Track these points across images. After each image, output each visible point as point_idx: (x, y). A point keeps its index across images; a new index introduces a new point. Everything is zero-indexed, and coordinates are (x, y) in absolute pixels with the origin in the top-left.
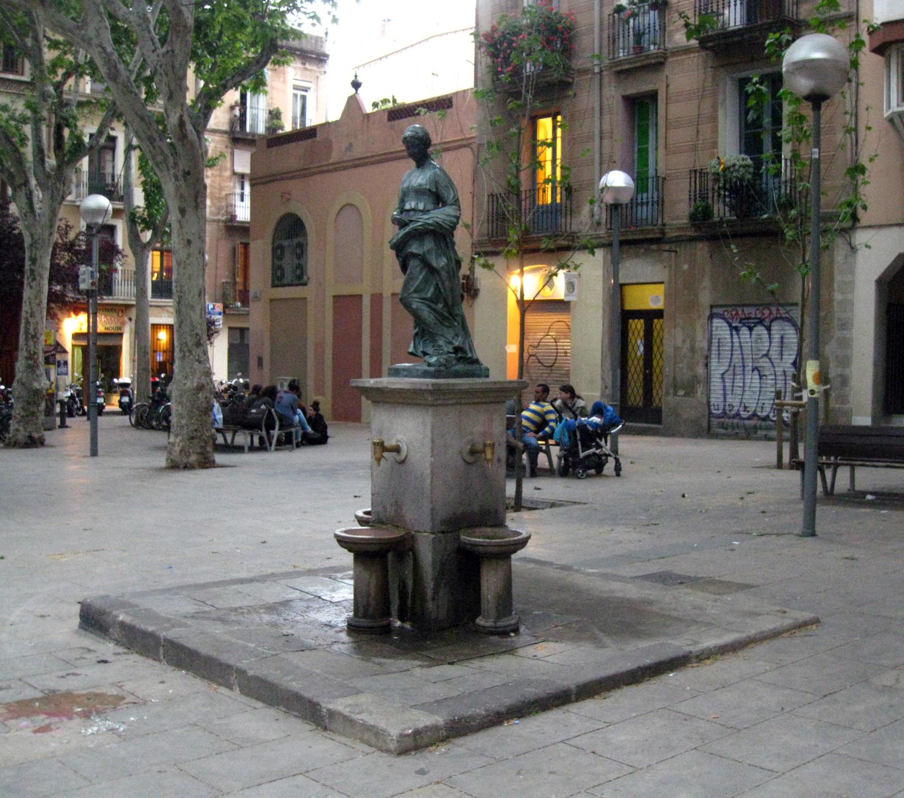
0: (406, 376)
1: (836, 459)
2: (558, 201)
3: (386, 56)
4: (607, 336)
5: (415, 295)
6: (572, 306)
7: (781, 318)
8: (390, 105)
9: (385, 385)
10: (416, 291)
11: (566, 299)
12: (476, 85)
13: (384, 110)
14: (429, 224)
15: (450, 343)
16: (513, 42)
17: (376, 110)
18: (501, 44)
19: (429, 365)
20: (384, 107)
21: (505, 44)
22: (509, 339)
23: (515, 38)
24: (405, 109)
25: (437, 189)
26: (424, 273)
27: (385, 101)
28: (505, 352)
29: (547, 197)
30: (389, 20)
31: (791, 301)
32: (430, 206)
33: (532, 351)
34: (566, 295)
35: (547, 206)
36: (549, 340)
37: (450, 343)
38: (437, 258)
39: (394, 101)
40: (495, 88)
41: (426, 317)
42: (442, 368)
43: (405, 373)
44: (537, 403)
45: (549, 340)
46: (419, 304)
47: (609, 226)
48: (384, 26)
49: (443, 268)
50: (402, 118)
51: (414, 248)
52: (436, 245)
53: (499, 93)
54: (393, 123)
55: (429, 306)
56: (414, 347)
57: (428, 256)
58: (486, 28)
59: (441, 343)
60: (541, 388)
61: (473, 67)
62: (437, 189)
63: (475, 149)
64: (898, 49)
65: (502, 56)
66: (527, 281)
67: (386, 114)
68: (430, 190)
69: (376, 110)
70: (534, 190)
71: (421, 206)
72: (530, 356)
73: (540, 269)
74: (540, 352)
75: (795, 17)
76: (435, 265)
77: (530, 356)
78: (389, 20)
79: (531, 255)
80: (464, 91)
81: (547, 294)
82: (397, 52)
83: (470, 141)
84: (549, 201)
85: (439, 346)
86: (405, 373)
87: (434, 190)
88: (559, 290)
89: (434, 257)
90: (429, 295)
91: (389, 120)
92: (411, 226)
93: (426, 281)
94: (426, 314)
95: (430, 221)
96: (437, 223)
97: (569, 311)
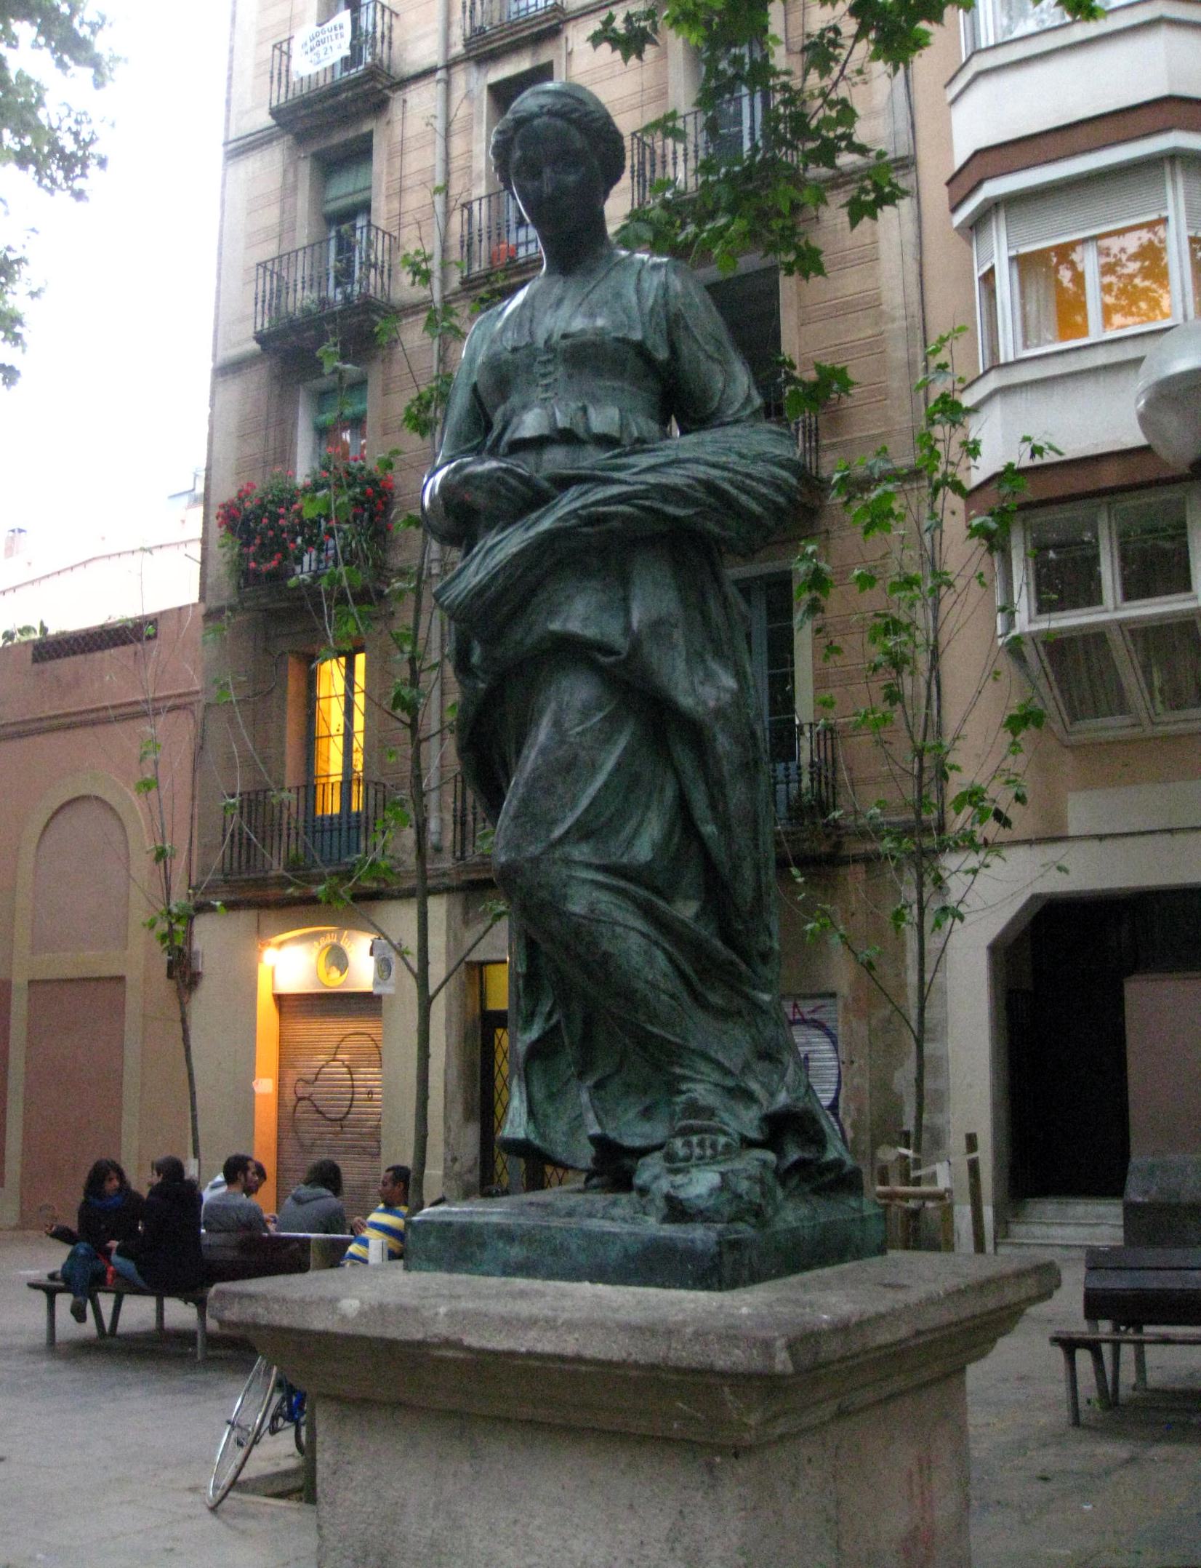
0: (526, 1269)
1: (1116, 1329)
2: (354, 808)
3: (14, 589)
4: (455, 1062)
5: (582, 852)
6: (385, 1005)
7: (804, 1021)
8: (36, 636)
9: (442, 1329)
10: (583, 831)
11: (376, 992)
12: (202, 597)
13: (26, 643)
14: (667, 492)
15: (748, 1097)
16: (280, 516)
17: (9, 643)
18: (258, 519)
19: (677, 1211)
20: (25, 639)
21: (265, 521)
22: (259, 1068)
23: (282, 511)
24: (67, 642)
25: (674, 350)
26: (622, 742)
27: (26, 630)
28: (252, 1093)
29: (331, 805)
30: (20, 531)
31: (823, 990)
32: (642, 425)
33: (302, 1091)
34: (376, 983)
35: (331, 818)
36: (337, 1071)
37: (748, 1097)
38: (695, 658)
39: (44, 630)
40: (241, 602)
41: (637, 960)
42: (745, 1230)
43: (516, 1252)
44: (389, 1209)
45: (337, 1071)
46: (605, 900)
47: (458, 854)
48: (12, 538)
49: (719, 713)
50: (59, 657)
51: (579, 614)
52: (683, 602)
53: (248, 610)
54: (41, 666)
55: (647, 911)
56: (531, 1113)
57: (653, 654)
58: (227, 492)
59: (702, 1092)
60: (391, 1173)
61: (197, 568)
62: (674, 350)
63: (199, 714)
64: (1024, 521)
65: (257, 541)
66: (290, 962)
67: (30, 650)
68: (640, 350)
69: (9, 643)
70: (309, 787)
71: (603, 419)
72: (300, 1099)
73: (316, 936)
74: (318, 1091)
75: (814, 472)
76: (686, 701)
77: (300, 1099)
78: (20, 531)
79: (302, 908)
80: (180, 609)
81: (335, 981)
82: (32, 582)
83: (187, 699)
84: (336, 810)
85: (694, 1109)
86: (516, 1252)
87: (662, 354)
88: (362, 971)
89: (681, 665)
90: (643, 851)
91: (35, 660)
92: (568, 503)
93: (627, 783)
94: (632, 944)
95: (674, 477)
96: (710, 487)
97: (380, 1015)
